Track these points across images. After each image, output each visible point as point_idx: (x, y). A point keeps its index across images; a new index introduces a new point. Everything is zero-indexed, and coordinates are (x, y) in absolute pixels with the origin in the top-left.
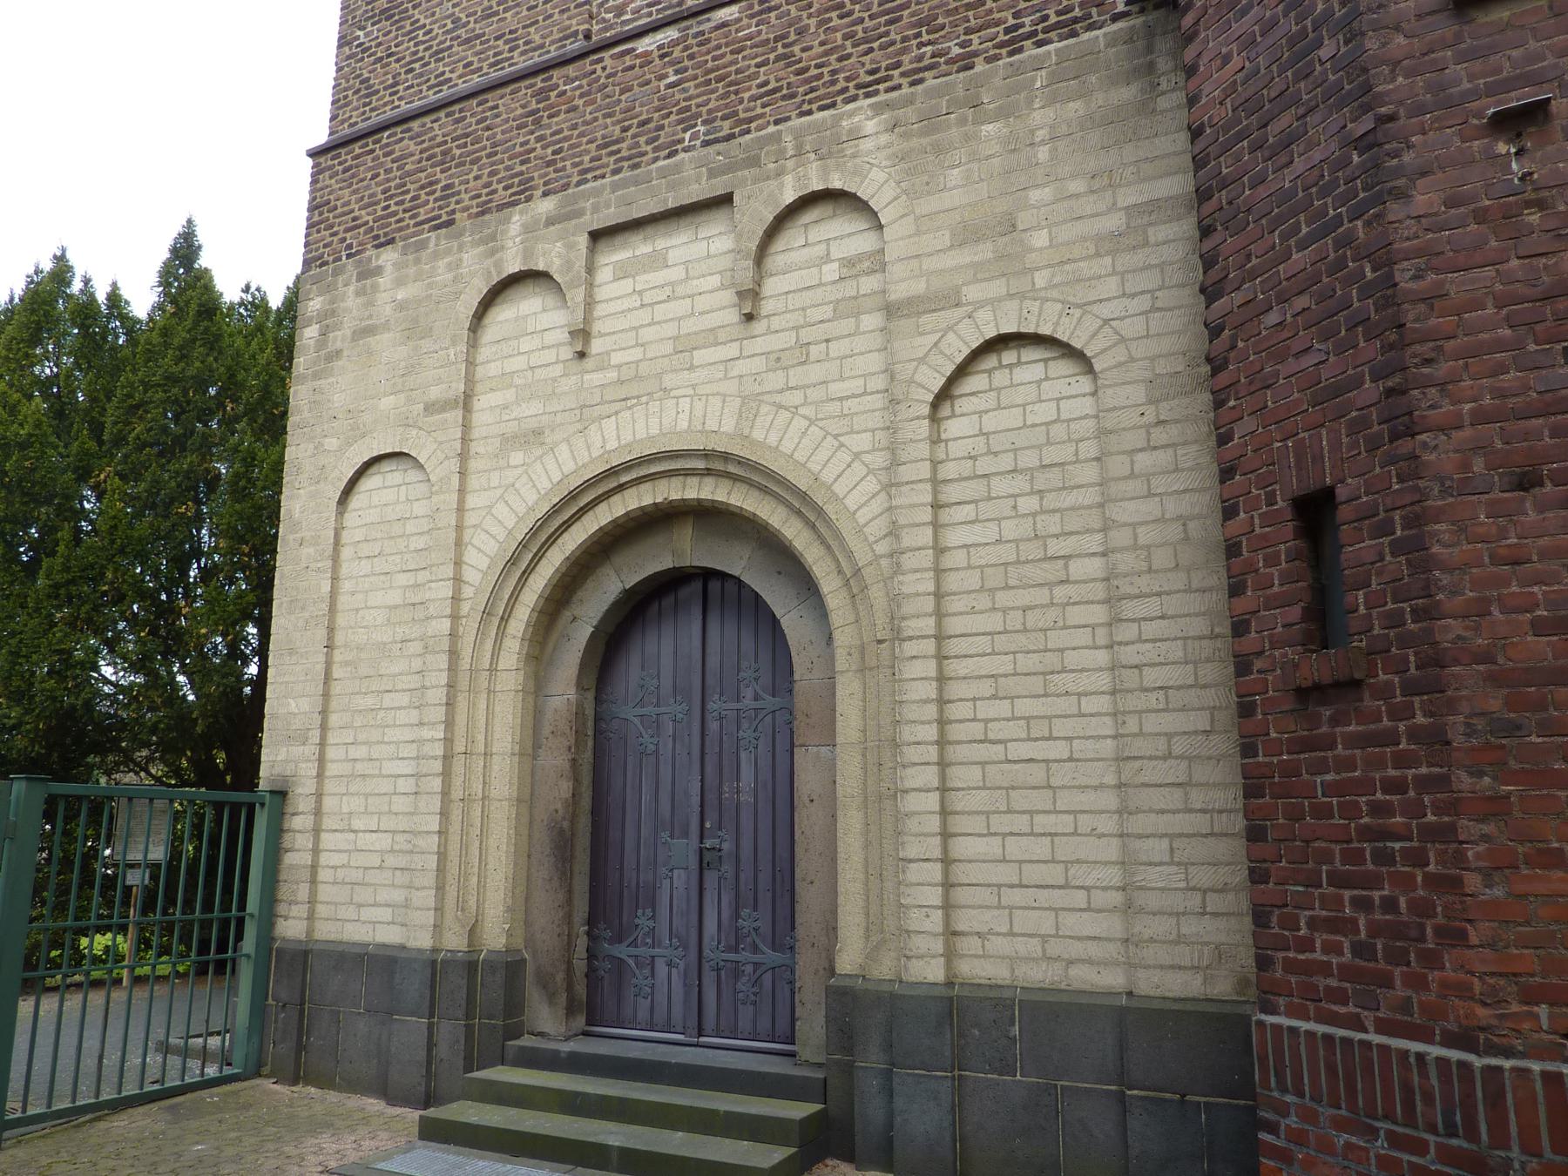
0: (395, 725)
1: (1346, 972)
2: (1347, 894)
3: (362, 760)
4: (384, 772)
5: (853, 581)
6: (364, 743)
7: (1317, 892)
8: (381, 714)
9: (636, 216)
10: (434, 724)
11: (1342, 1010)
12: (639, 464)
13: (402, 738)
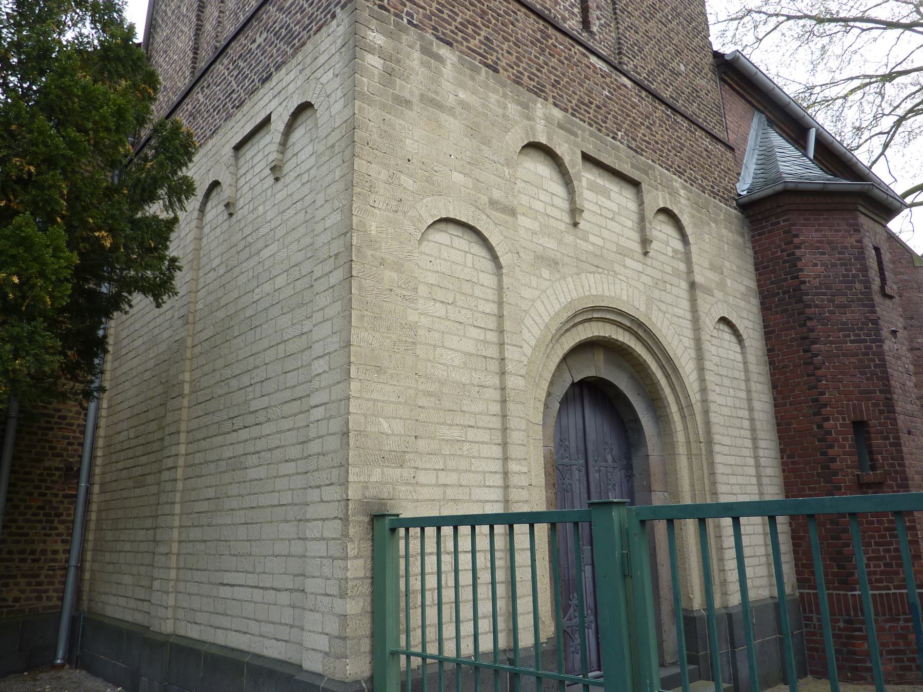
0: (480, 457)
1: (882, 573)
2: (881, 548)
3: (453, 486)
4: (473, 498)
5: (686, 409)
6: (453, 470)
7: (870, 548)
8: (466, 446)
9: (602, 160)
10: (520, 460)
11: (882, 585)
12: (604, 310)
13: (487, 469)
